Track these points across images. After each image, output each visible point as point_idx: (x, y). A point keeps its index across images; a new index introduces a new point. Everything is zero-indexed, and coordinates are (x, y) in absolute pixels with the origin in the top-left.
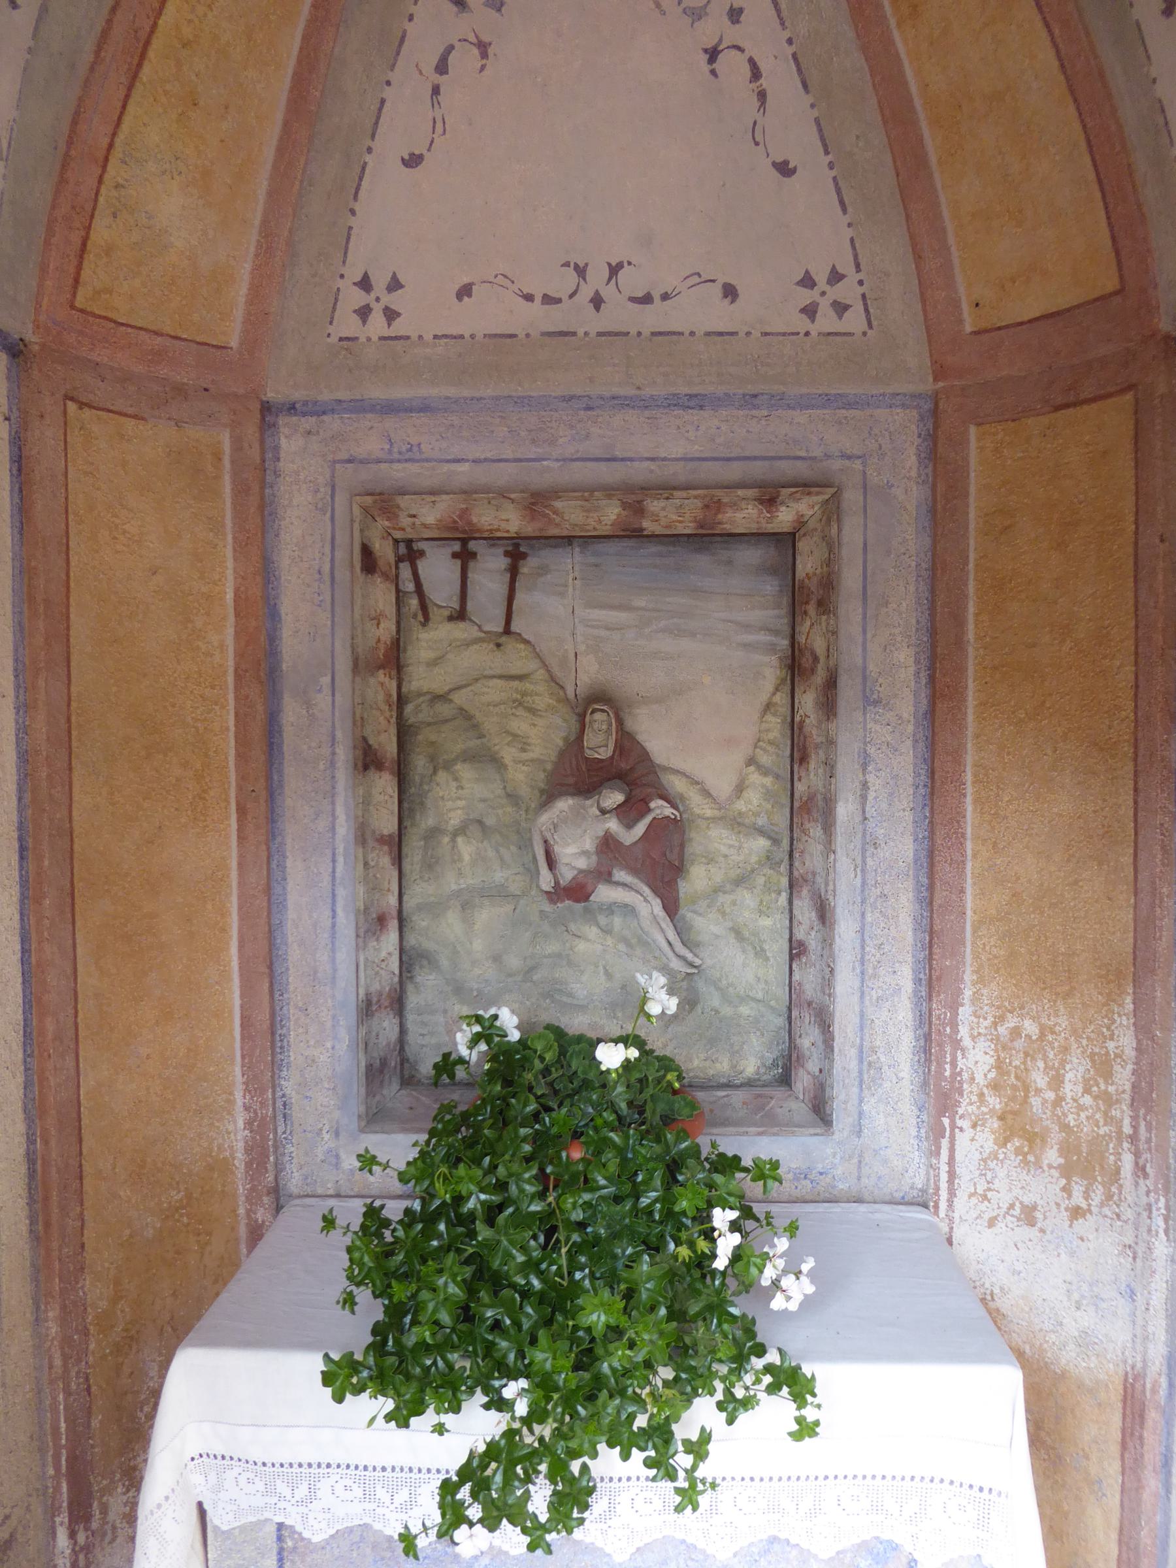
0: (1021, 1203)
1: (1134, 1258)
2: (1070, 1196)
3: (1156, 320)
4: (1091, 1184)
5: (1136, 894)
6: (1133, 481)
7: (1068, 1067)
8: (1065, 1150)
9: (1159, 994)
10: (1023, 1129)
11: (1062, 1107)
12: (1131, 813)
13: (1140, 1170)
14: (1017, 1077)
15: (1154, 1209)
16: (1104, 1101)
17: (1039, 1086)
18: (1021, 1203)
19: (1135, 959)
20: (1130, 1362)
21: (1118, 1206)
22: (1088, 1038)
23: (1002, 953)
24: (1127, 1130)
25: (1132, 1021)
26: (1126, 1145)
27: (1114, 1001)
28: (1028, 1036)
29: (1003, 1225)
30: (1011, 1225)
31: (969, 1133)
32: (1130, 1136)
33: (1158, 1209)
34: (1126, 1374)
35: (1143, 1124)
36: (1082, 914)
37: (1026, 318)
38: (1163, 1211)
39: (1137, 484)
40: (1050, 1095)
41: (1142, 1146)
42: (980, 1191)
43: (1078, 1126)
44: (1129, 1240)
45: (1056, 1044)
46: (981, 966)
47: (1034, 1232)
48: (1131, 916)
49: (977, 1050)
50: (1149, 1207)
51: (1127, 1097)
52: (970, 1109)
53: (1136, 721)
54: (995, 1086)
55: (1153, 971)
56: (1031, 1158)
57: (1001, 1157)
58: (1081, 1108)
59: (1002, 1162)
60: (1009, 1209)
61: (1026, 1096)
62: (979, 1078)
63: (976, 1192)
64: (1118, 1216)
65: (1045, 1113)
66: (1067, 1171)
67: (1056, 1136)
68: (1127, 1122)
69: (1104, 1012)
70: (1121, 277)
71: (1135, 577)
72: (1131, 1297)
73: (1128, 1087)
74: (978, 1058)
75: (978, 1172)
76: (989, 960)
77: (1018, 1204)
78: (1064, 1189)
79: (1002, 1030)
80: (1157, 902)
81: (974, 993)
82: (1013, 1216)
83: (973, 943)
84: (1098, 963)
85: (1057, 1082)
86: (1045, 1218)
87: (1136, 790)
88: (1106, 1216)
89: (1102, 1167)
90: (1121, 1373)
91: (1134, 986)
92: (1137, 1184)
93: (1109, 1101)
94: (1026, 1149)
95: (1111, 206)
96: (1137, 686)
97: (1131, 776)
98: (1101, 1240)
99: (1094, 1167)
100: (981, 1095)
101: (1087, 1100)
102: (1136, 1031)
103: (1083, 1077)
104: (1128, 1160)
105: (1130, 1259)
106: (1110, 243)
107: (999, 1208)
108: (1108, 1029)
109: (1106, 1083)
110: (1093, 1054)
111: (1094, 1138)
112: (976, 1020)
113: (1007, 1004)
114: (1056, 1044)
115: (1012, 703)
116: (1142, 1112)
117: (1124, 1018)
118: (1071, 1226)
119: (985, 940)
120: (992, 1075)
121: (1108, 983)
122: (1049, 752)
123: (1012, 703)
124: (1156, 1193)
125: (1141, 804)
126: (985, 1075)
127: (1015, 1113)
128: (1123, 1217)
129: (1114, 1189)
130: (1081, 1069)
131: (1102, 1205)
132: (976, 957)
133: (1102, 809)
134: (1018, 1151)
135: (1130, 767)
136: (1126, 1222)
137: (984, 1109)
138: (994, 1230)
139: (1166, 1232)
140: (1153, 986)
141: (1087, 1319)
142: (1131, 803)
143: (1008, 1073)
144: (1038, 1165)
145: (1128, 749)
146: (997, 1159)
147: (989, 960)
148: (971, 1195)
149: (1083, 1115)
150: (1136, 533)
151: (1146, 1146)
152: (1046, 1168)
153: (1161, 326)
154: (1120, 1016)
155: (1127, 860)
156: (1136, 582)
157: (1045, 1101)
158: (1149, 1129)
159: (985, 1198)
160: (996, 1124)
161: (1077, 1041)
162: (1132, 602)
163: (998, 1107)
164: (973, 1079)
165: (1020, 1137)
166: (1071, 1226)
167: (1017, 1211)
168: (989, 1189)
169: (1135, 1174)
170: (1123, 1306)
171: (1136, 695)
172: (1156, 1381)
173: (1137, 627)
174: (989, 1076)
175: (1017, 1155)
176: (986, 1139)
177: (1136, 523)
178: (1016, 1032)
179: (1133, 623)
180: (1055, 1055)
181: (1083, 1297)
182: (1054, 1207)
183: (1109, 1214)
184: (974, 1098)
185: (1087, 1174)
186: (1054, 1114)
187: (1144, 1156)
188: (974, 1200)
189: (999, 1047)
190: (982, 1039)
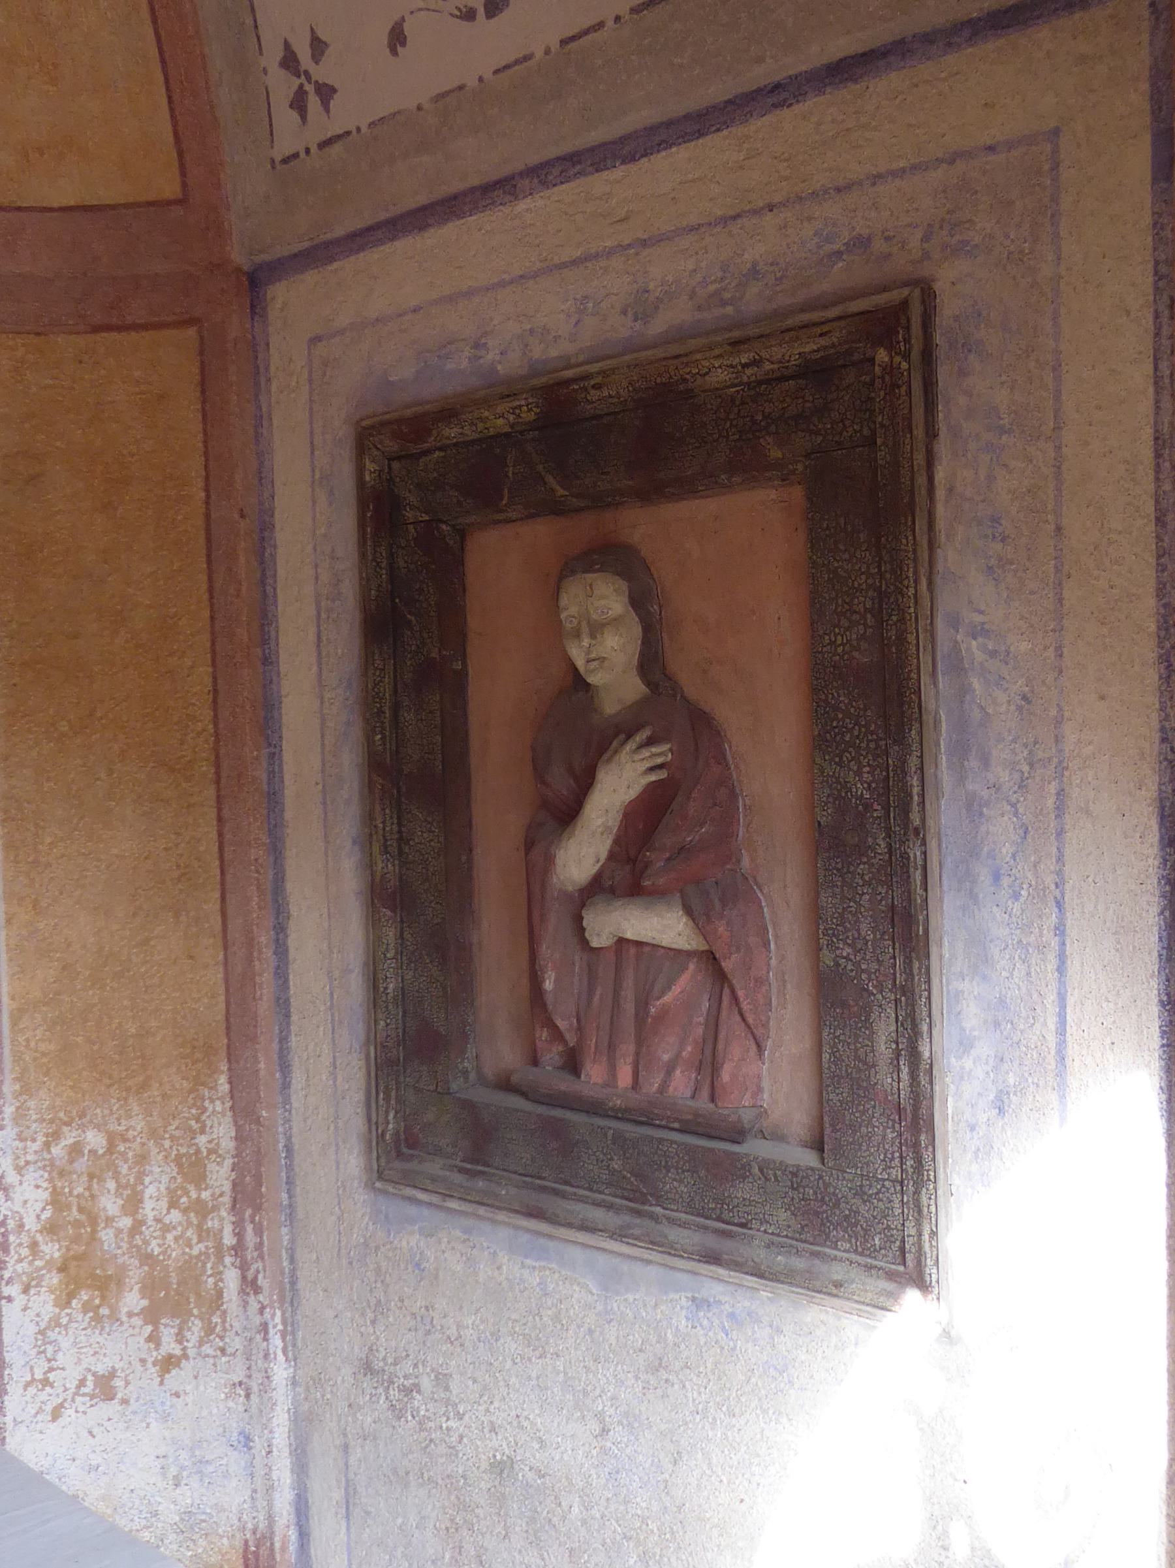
0: (94, 1374)
1: (248, 1396)
2: (158, 1345)
3: (228, 248)
4: (184, 1322)
5: (226, 948)
6: (200, 437)
7: (147, 1180)
8: (149, 1288)
9: (262, 1065)
10: (93, 1276)
11: (141, 1233)
12: (216, 849)
13: (250, 1285)
14: (81, 1210)
15: (270, 1326)
16: (197, 1213)
17: (110, 1213)
18: (94, 1374)
19: (228, 1028)
20: (250, 1526)
21: (222, 1338)
22: (172, 1138)
23: (52, 1047)
24: (229, 1240)
25: (228, 1105)
26: (228, 1260)
27: (203, 1084)
28: (93, 1152)
29: (71, 1412)
30: (81, 1409)
31: (20, 1300)
32: (233, 1248)
33: (275, 1326)
34: (246, 1542)
35: (249, 1228)
36: (156, 980)
37: (55, 205)
38: (280, 1327)
39: (205, 442)
40: (126, 1222)
41: (250, 1254)
42: (39, 1376)
43: (164, 1253)
44: (239, 1375)
45: (131, 1154)
46: (24, 1071)
47: (114, 1407)
48: (220, 976)
49: (25, 1185)
50: (264, 1328)
51: (226, 1199)
52: (19, 1268)
53: (217, 734)
54: (51, 1229)
55: (254, 1039)
56: (104, 1311)
57: (64, 1321)
58: (167, 1229)
59: (66, 1327)
60: (78, 1387)
61: (94, 1232)
62: (31, 1224)
63: (33, 1380)
64: (223, 1351)
65: (119, 1248)
66: (152, 1315)
67: (136, 1273)
68: (228, 1230)
69: (190, 1101)
70: (184, 185)
71: (209, 556)
72: (245, 1445)
73: (227, 1187)
74: (27, 1196)
75: (34, 1352)
76: (35, 1059)
77: (90, 1377)
78: (150, 1339)
79: (57, 1151)
80: (255, 954)
81: (18, 1108)
82: (84, 1395)
83: (13, 1041)
84: (180, 1040)
85: (133, 1203)
86: (127, 1383)
87: (220, 819)
88: (207, 1356)
89: (198, 1295)
90: (239, 1543)
91: (229, 1061)
92: (246, 1304)
93: (202, 1210)
94: (97, 1301)
95: (176, 97)
96: (216, 691)
97: (213, 803)
98: (202, 1388)
99: (188, 1299)
100: (34, 1246)
101: (175, 1216)
102: (234, 1116)
103: (167, 1188)
104: (232, 1279)
105: (242, 1399)
106: (171, 139)
107: (66, 1390)
108: (198, 1120)
109: (199, 1189)
110: (179, 1157)
111: (186, 1262)
112: (21, 1145)
113: (61, 1115)
114: (131, 1154)
115: (51, 711)
116: (248, 1212)
117: (218, 1103)
118: (161, 1383)
119: (29, 1034)
120: (47, 1214)
121: (194, 1063)
122: (103, 775)
123: (51, 711)
124: (272, 1307)
125: (228, 836)
126: (38, 1217)
127: (78, 1258)
128: (229, 1351)
129: (216, 1319)
130: (165, 1179)
131: (201, 1343)
132: (18, 1058)
133: (177, 845)
134: (86, 1307)
135: (211, 792)
136: (234, 1355)
137: (38, 1263)
138: (61, 1421)
139: (285, 1351)
140: (256, 1058)
141: (186, 1496)
142: (214, 835)
143: (68, 1207)
144: (114, 1318)
145: (207, 769)
146: (59, 1325)
147: (35, 1059)
148: (27, 1385)
149: (170, 1237)
150: (207, 502)
151: (255, 1254)
152: (124, 1319)
153: (233, 256)
154: (212, 1101)
155: (212, 906)
156: (209, 562)
157: (119, 1231)
158: (259, 1231)
159: (46, 1382)
160: (55, 1279)
161: (157, 1144)
162: (205, 586)
163: (57, 1255)
164: (21, 1226)
165: (89, 1287)
166: (161, 1383)
167: (89, 1387)
168: (51, 1370)
169: (242, 1292)
170: (235, 1461)
171: (215, 702)
172: (285, 1536)
173: (212, 618)
174: (43, 1217)
175: (85, 1313)
176: (44, 1304)
177: (207, 490)
178: (76, 1150)
179: (206, 613)
180: (130, 1168)
181: (183, 1468)
182: (137, 1365)
183: (210, 1351)
184: (25, 1252)
185: (180, 1311)
186: (131, 1245)
187: (254, 1267)
188: (32, 1390)
189: (55, 1174)
190: (31, 1168)
